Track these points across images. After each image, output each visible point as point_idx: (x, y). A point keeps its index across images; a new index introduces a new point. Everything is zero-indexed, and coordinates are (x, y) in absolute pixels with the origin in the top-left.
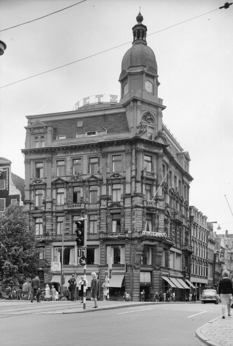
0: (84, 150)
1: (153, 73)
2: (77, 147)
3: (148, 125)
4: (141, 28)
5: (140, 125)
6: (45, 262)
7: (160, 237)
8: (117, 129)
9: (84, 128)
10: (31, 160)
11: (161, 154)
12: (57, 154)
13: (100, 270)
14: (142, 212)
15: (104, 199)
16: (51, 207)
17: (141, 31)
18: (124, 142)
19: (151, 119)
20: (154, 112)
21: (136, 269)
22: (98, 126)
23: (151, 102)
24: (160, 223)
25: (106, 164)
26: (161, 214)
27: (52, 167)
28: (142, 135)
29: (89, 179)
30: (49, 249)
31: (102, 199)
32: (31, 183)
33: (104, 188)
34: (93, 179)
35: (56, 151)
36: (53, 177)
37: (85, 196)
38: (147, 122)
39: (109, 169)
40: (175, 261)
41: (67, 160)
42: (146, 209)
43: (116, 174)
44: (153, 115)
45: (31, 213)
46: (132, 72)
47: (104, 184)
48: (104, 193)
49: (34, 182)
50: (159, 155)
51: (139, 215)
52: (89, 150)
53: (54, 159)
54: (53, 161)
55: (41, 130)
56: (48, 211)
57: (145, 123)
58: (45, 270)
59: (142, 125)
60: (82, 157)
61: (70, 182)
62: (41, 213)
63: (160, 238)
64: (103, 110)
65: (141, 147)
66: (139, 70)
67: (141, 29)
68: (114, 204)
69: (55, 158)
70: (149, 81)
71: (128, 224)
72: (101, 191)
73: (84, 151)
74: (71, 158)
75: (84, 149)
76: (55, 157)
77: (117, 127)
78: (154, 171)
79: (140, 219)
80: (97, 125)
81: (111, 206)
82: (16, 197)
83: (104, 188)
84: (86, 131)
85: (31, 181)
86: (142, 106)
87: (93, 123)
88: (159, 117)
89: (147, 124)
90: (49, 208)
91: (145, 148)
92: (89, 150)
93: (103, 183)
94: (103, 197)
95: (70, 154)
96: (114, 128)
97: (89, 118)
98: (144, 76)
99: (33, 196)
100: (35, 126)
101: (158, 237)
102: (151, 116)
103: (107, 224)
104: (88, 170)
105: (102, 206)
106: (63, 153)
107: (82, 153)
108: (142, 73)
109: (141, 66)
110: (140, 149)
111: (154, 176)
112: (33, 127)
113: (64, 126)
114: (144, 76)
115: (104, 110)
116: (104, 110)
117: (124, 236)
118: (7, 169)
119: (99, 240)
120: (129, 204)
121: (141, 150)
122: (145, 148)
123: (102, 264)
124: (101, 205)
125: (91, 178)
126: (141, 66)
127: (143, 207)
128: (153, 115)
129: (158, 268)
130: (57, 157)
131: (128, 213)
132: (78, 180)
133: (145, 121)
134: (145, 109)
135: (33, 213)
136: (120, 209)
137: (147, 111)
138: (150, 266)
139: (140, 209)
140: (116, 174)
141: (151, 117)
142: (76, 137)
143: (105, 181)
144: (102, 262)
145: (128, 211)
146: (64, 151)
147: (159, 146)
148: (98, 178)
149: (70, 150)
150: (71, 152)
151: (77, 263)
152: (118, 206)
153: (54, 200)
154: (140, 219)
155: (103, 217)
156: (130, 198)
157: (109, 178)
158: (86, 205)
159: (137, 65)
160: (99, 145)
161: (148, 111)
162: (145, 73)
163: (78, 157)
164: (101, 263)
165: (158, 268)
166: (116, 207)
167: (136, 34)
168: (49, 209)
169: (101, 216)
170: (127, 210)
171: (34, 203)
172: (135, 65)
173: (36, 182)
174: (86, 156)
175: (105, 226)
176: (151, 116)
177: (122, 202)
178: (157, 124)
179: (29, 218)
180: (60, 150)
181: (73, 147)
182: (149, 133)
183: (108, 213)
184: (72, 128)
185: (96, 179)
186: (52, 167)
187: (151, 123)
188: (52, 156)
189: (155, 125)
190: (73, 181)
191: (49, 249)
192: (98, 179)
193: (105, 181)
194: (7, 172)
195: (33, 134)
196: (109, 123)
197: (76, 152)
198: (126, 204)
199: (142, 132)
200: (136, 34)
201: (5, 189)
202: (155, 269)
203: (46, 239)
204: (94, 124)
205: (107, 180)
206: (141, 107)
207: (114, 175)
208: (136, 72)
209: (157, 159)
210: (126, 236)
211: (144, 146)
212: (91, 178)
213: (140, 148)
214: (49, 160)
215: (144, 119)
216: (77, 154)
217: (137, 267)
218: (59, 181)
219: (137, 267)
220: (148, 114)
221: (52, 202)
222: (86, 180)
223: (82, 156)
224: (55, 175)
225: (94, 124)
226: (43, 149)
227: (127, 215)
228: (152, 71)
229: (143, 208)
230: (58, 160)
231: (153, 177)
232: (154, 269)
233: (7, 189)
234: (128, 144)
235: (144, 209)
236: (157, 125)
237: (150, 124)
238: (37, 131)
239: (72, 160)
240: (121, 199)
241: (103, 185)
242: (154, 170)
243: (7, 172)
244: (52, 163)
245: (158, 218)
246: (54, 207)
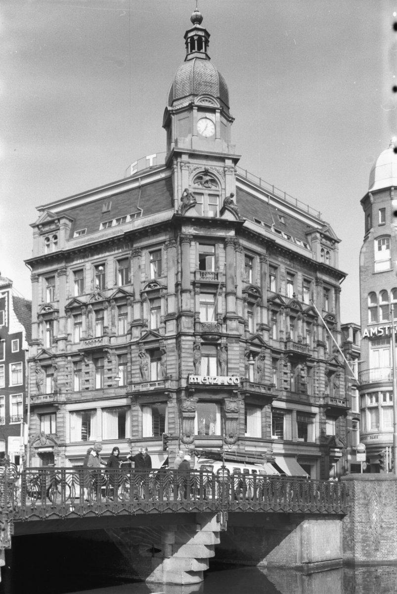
0: (110, 249)
1: (212, 103)
2: (121, 239)
3: (207, 192)
4: (195, 34)
5: (185, 194)
6: (56, 438)
7: (226, 384)
8: (157, 206)
9: (112, 213)
10: (39, 275)
11: (231, 238)
12: (73, 261)
13: (132, 447)
14: (192, 343)
15: (137, 326)
16: (64, 348)
17: (196, 38)
18: (163, 227)
19: (213, 181)
20: (217, 168)
21: (186, 443)
22: (131, 206)
23: (208, 152)
24: (231, 359)
25: (140, 267)
26: (233, 343)
27: (67, 282)
28: (186, 211)
29: (115, 295)
30: (61, 415)
31: (134, 326)
32: (39, 312)
33: (172, 301)
34: (120, 295)
35: (71, 256)
36: (68, 299)
37: (110, 323)
38: (205, 188)
39: (143, 275)
40: (382, 413)
41: (87, 269)
42: (199, 337)
43: (152, 283)
44: (215, 173)
45: (38, 360)
46: (176, 109)
47: (137, 300)
48: (137, 316)
49: (42, 309)
50: (226, 240)
51: (186, 349)
52: (116, 248)
53: (69, 269)
54: (68, 273)
55: (53, 227)
56: (59, 354)
57: (199, 188)
58: (56, 451)
59: (188, 194)
60: (106, 260)
61: (89, 304)
62: (50, 358)
63: (225, 385)
64: (138, 178)
65: (189, 230)
66: (186, 103)
67: (196, 35)
68: (151, 333)
69: (70, 268)
70: (206, 118)
71: (171, 365)
72: (133, 314)
73: (109, 251)
74: (115, 258)
75: (109, 248)
76: (69, 266)
77: (158, 204)
78: (219, 269)
79: (189, 355)
80: (130, 205)
81: (146, 336)
82: (18, 335)
83: (172, 301)
84: (113, 218)
85: (144, 285)
86: (191, 162)
87: (125, 202)
88: (227, 176)
89: (206, 190)
90: (62, 349)
91: (197, 232)
92: (116, 248)
93: (134, 299)
94: (134, 323)
95: (90, 258)
96: (153, 205)
97: (120, 195)
98: (195, 111)
99: (42, 332)
100: (45, 219)
101: (223, 385)
102: (213, 176)
103: (141, 369)
104: (115, 281)
105: (134, 338)
106: (81, 259)
107: (107, 254)
108: (190, 107)
109: (190, 95)
110: (186, 235)
111: (217, 279)
112: (41, 222)
113: (86, 214)
114: (195, 111)
115: (140, 179)
116: (140, 179)
117: (162, 386)
118: (7, 293)
119: (126, 396)
120: (173, 331)
121: (188, 236)
122: (197, 232)
123: (134, 438)
124: (167, 331)
125: (118, 293)
126: (190, 95)
127: (194, 333)
128: (214, 173)
129: (232, 440)
130: (73, 265)
131: (171, 346)
132: (101, 299)
133: (200, 186)
134: (199, 166)
135: (41, 360)
136: (158, 340)
137: (203, 167)
138: (217, 438)
139: (190, 338)
140: (152, 283)
141: (211, 176)
142: (99, 229)
143: (138, 297)
144: (134, 434)
145: (172, 343)
146: (82, 254)
147: (226, 225)
148: (127, 293)
149: (90, 252)
150: (92, 255)
151: (101, 438)
152: (155, 335)
153: (68, 335)
154: (189, 355)
155: (135, 357)
156: (175, 321)
157: (143, 291)
158: (112, 339)
159: (183, 96)
160: (127, 238)
161: (205, 168)
162: (196, 106)
163: (75, 268)
164: (133, 436)
165: (232, 440)
166: (153, 338)
167: (189, 44)
168: (63, 350)
169: (133, 355)
170: (170, 341)
171: (43, 343)
172: (181, 96)
173: (150, 286)
174: (112, 257)
175: (138, 371)
176: (213, 176)
177: (162, 328)
178: (223, 187)
179: (140, 351)
180: (77, 253)
181: (121, 238)
182: (209, 205)
183: (142, 350)
184: (96, 215)
185: (125, 294)
186: (67, 282)
187: (213, 188)
188: (67, 265)
189: (220, 189)
190: (94, 301)
191: (61, 415)
192: (128, 294)
193: (138, 297)
194: (7, 298)
195: (42, 234)
196: (147, 198)
197: (98, 254)
198: (169, 332)
199: (186, 205)
200: (189, 44)
201: (4, 325)
202: (226, 443)
203: (55, 400)
204: (126, 204)
205: (141, 294)
206: (189, 163)
207: (149, 283)
208: (182, 108)
209: (225, 248)
210: (165, 387)
211: (195, 229)
212: (118, 293)
213: (187, 233)
214: (62, 272)
215: (197, 182)
216: (100, 256)
217: (186, 439)
218: (76, 304)
219: (186, 439)
220: (206, 172)
221: (65, 339)
222: (110, 297)
223: (105, 259)
224: (71, 295)
225: (126, 204)
226: (96, 245)
227: (170, 349)
228: (210, 101)
229: (194, 335)
230: (96, 264)
231: (216, 280)
232: (224, 443)
233: (7, 325)
234: (169, 229)
235: (196, 337)
236: (225, 189)
237: (210, 190)
238: (47, 229)
239: (93, 267)
240: (161, 323)
241: (135, 303)
242: (218, 267)
243: (7, 298)
244: (67, 276)
245: (227, 351)
246: (69, 347)
